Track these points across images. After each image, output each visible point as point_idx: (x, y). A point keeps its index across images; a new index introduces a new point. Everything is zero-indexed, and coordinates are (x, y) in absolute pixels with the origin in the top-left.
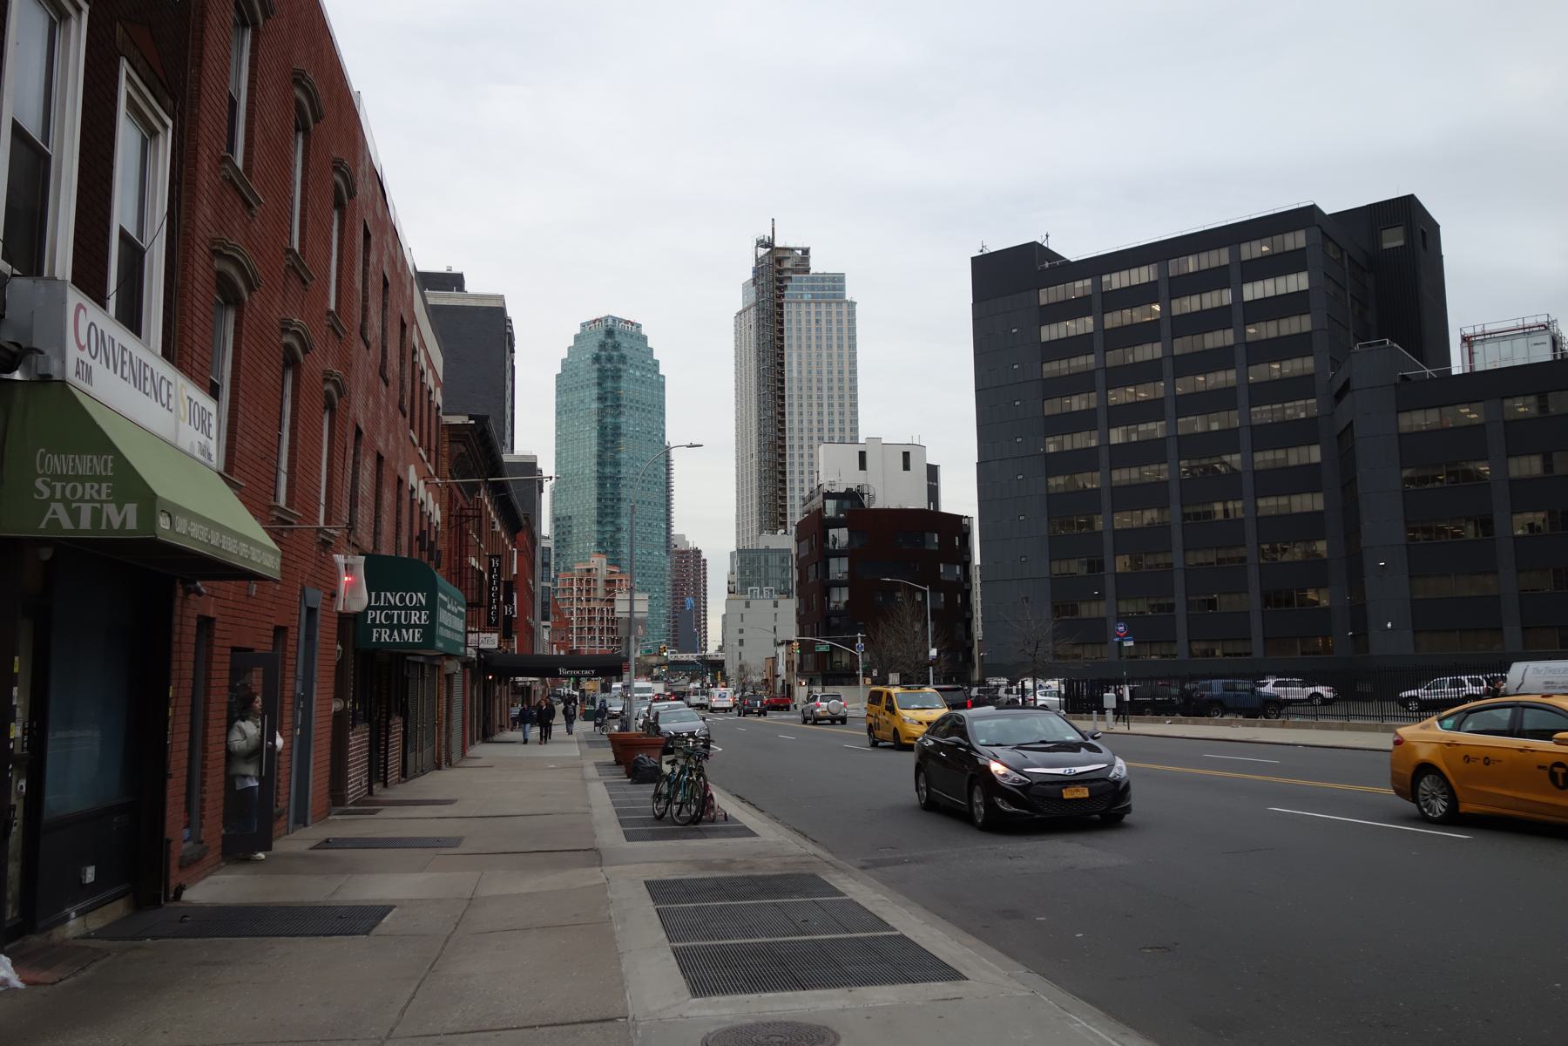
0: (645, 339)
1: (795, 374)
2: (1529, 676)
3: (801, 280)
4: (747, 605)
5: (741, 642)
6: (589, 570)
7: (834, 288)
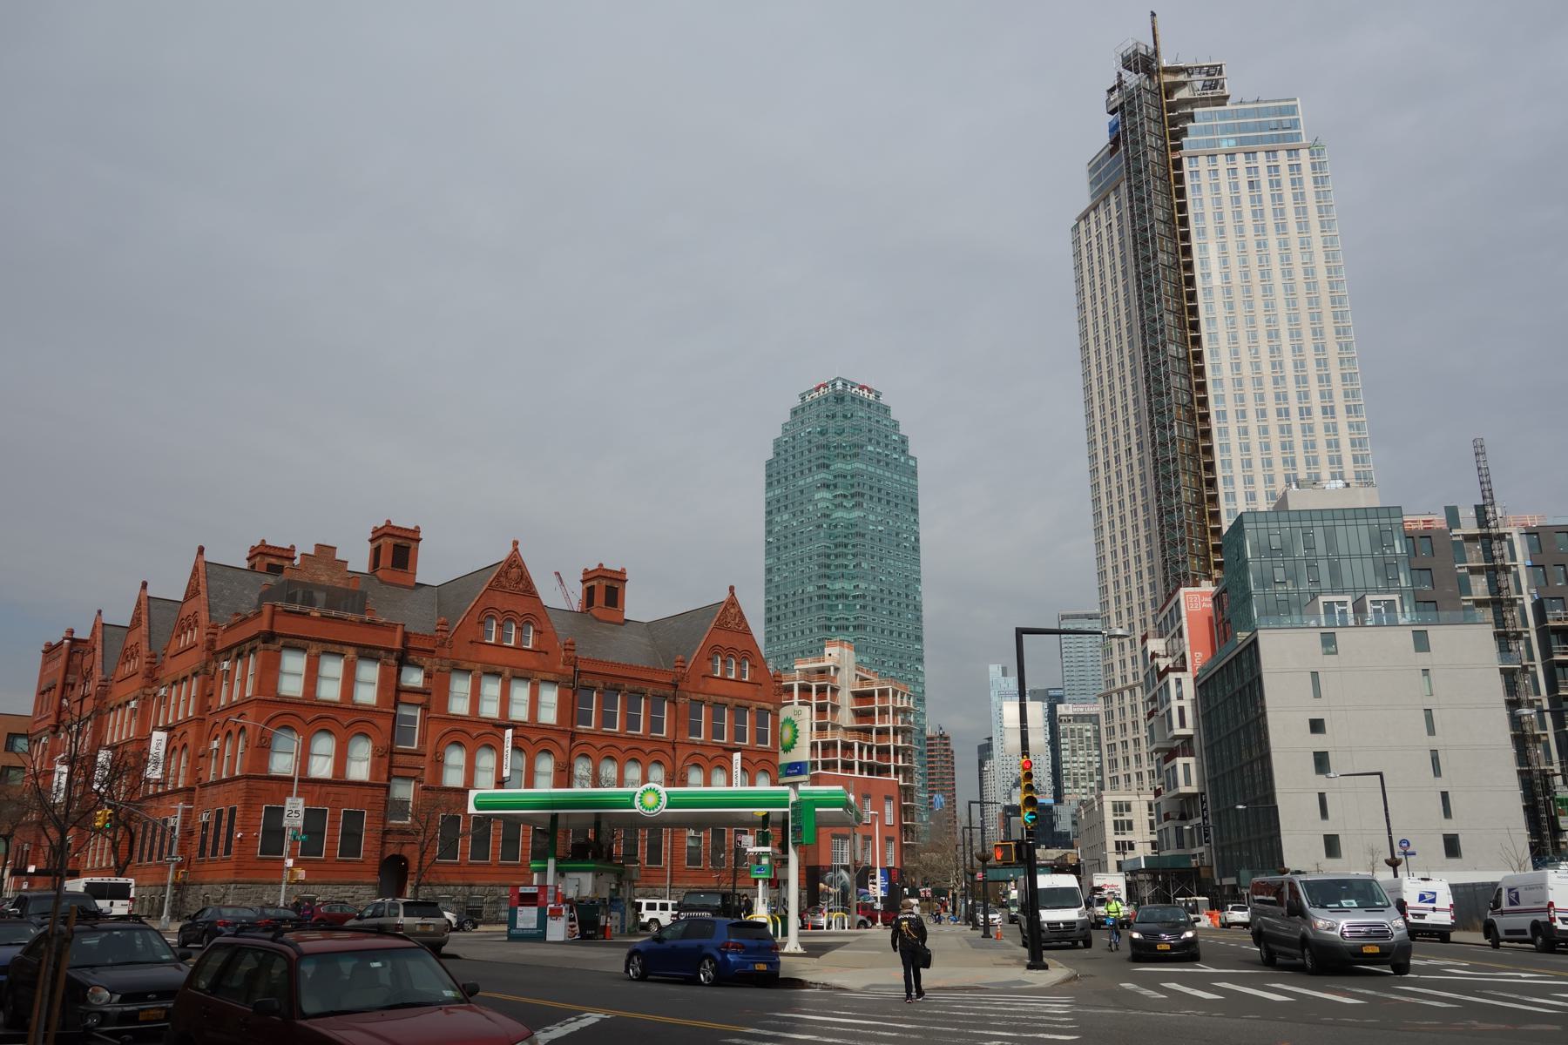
0: (887, 409)
1: (1216, 280)
2: (16, 951)
3: (1211, 117)
4: (1329, 641)
5: (1322, 762)
6: (822, 672)
7: (1280, 126)
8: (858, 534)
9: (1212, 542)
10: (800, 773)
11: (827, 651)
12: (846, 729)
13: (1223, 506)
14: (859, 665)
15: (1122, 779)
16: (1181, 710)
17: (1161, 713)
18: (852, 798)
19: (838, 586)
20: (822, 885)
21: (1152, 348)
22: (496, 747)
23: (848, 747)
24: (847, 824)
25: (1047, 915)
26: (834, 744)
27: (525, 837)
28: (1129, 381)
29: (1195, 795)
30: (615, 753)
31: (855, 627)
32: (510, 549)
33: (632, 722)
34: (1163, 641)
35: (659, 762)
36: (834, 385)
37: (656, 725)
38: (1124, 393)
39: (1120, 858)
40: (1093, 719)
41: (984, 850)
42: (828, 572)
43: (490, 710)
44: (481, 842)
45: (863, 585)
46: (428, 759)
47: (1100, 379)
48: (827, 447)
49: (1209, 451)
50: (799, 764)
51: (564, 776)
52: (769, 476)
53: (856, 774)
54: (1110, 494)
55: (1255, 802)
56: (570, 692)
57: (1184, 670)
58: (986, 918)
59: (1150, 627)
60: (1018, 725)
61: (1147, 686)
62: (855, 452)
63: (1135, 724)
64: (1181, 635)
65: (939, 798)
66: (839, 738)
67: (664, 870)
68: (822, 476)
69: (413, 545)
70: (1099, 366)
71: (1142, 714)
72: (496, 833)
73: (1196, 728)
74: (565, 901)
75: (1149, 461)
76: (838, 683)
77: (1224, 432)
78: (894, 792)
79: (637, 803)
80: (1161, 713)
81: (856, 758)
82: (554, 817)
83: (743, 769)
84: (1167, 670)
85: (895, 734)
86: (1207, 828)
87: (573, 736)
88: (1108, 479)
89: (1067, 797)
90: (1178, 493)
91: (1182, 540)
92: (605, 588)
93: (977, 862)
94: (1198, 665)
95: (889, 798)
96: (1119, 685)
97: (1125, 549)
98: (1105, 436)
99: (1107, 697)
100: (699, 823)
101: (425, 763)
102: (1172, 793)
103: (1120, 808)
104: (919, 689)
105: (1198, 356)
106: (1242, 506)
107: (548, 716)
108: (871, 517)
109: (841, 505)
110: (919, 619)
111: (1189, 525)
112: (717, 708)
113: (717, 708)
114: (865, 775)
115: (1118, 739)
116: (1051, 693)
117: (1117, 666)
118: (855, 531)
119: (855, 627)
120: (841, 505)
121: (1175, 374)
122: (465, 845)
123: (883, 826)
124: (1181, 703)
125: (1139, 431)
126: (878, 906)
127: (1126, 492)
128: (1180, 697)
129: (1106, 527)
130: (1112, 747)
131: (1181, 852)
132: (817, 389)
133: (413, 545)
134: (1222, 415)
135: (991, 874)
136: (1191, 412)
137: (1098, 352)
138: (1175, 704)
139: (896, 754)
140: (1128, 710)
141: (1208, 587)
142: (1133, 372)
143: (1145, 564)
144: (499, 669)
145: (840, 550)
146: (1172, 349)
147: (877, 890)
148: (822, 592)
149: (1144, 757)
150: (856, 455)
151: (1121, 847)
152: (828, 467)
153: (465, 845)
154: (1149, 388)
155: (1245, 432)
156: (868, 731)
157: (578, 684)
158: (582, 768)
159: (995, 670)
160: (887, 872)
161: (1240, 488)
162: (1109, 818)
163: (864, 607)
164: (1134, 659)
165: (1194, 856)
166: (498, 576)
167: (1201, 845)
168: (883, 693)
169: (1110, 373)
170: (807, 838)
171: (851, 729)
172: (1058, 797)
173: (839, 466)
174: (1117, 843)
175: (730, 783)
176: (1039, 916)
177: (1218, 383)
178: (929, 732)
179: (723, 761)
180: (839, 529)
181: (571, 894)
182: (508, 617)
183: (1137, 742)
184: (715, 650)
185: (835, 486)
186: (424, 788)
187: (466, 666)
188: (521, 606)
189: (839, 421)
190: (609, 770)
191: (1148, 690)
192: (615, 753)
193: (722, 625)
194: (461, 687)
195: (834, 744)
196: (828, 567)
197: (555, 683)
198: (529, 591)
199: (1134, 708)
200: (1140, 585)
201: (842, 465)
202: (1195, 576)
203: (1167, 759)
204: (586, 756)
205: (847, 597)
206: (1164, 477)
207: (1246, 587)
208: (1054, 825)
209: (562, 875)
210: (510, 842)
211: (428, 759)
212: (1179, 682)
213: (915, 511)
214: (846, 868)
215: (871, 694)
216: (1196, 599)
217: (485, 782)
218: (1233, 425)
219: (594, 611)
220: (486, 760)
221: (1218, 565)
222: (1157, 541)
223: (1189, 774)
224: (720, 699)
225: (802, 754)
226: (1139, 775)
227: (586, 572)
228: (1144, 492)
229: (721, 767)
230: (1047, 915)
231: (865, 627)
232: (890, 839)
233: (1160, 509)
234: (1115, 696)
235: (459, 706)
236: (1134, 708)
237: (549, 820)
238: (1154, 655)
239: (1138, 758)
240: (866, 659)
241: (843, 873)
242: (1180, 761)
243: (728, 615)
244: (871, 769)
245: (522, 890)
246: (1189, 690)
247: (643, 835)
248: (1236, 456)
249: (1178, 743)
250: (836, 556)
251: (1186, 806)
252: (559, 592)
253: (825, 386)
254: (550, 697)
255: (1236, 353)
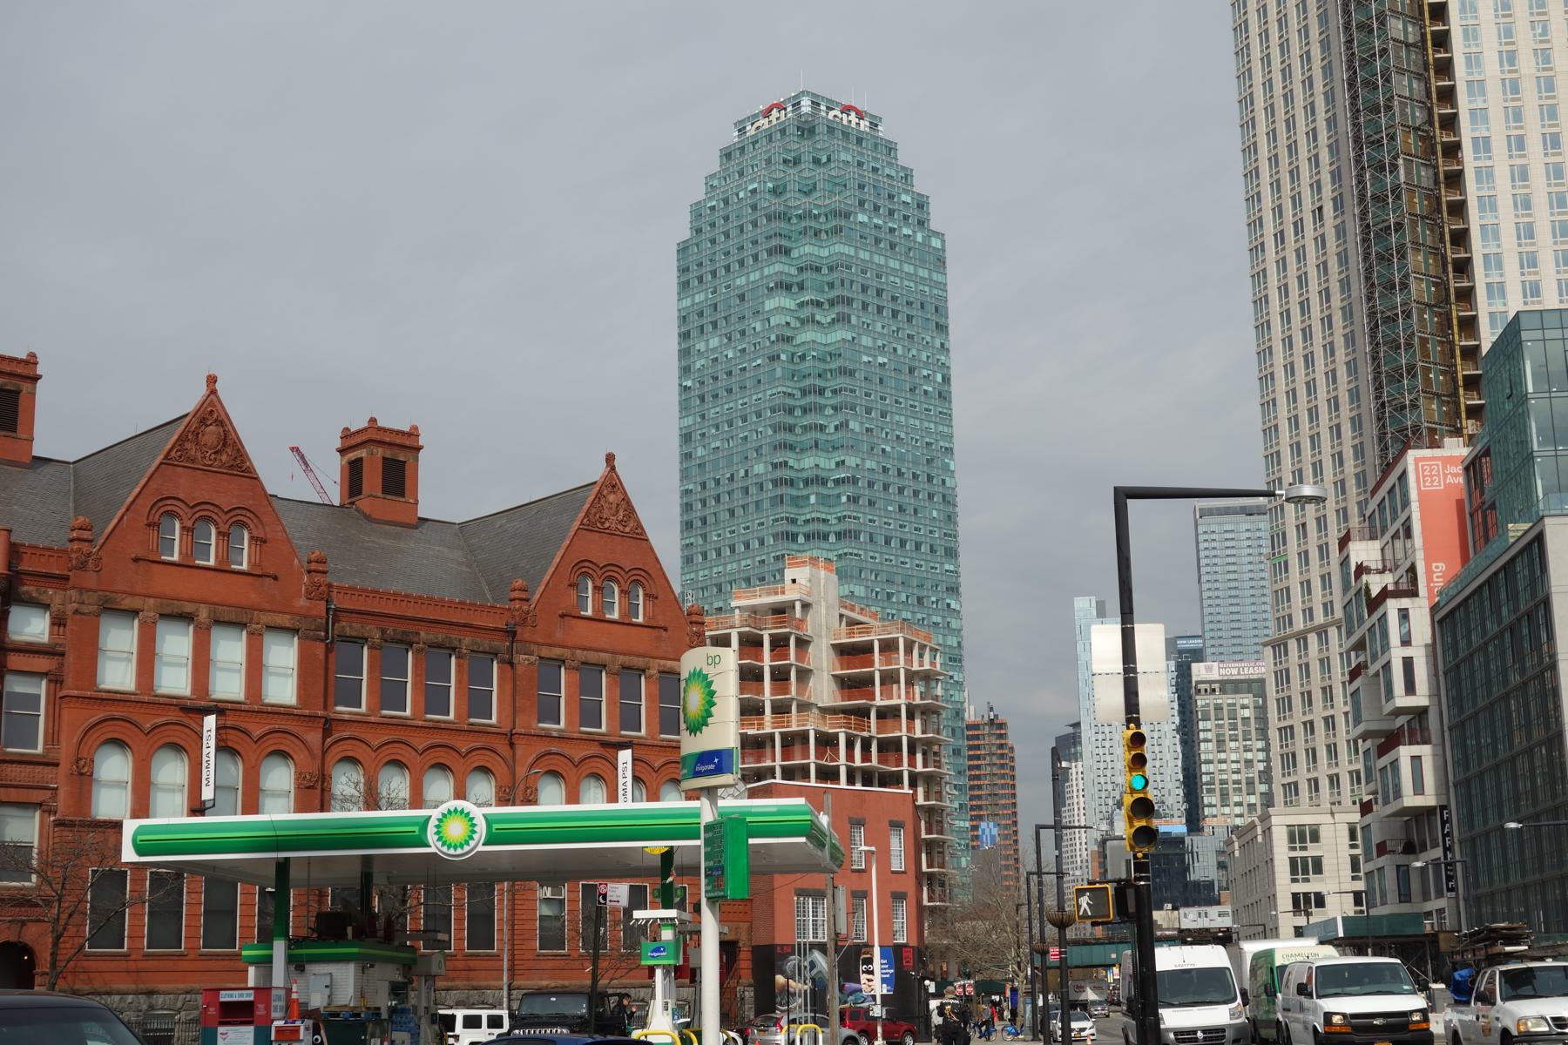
0: (891, 148)
6: (780, 611)
8: (844, 371)
9: (1463, 370)
10: (719, 770)
11: (789, 574)
12: (825, 711)
13: (1484, 307)
14: (846, 601)
15: (1304, 787)
16: (1408, 663)
17: (1372, 670)
18: (824, 820)
19: (808, 462)
20: (780, 979)
21: (1361, 26)
22: (188, 747)
23: (827, 742)
24: (821, 865)
25: (1173, 1018)
26: (804, 736)
27: (247, 904)
28: (1319, 86)
29: (1430, 811)
30: (404, 754)
31: (839, 535)
32: (202, 391)
33: (437, 700)
34: (1377, 545)
35: (485, 770)
36: (797, 105)
37: (479, 704)
38: (1311, 109)
39: (1301, 921)
40: (1255, 687)
41: (1061, 908)
42: (790, 438)
43: (175, 680)
44: (166, 914)
45: (852, 461)
46: (63, 770)
47: (1268, 84)
48: (784, 217)
49: (1459, 209)
50: (718, 753)
51: (314, 792)
52: (684, 270)
53: (843, 784)
54: (1284, 290)
55: (1537, 817)
56: (320, 649)
57: (1413, 594)
58: (1066, 1029)
59: (1355, 521)
60: (1120, 667)
61: (1348, 625)
62: (837, 223)
63: (1327, 692)
64: (1408, 533)
65: (989, 829)
66: (812, 725)
67: (498, 957)
68: (777, 268)
69: (25, 387)
70: (1266, 60)
71: (1338, 673)
72: (193, 900)
73: (1435, 693)
74: (306, 1014)
75: (1354, 229)
76: (809, 630)
77: (1486, 175)
78: (906, 815)
79: (431, 836)
80: (1372, 670)
81: (842, 759)
82: (283, 867)
83: (636, 779)
84: (1385, 594)
85: (911, 717)
86: (1450, 865)
87: (328, 726)
88: (1282, 264)
89: (1209, 822)
90: (1405, 286)
91: (1411, 369)
92: (382, 464)
93: (1051, 931)
94: (1439, 583)
95: (896, 825)
96: (1299, 624)
97: (1311, 387)
98: (1276, 185)
99: (1279, 646)
100: (554, 871)
101: (59, 778)
102: (1393, 807)
103: (1302, 836)
104: (952, 641)
105: (1442, 40)
106: (1515, 303)
107: (282, 689)
108: (866, 341)
109: (811, 320)
110: (950, 519)
111: (1424, 341)
112: (589, 670)
113: (589, 670)
114: (858, 787)
115: (1297, 718)
116: (1182, 644)
117: (1296, 591)
118: (838, 365)
119: (839, 535)
120: (811, 320)
121: (1401, 71)
122: (136, 923)
123: (886, 873)
124: (1408, 652)
125: (1336, 176)
126: (877, 1011)
127: (1314, 286)
128: (1406, 642)
129: (1278, 347)
130: (1287, 732)
131: (1405, 908)
132: (767, 113)
133: (25, 387)
134: (1483, 145)
135: (1076, 955)
136: (1428, 140)
137: (1265, 35)
138: (1397, 654)
139: (912, 752)
140: (1315, 668)
141: (1456, 449)
142: (1327, 70)
143: (1346, 411)
144: (189, 608)
145: (811, 399)
146: (1396, 27)
147: (875, 983)
148: (779, 473)
149: (1343, 749)
150: (837, 230)
151: (1302, 903)
152: (787, 252)
153: (136, 923)
154: (1354, 98)
155: (1523, 174)
156: (863, 713)
157: (336, 632)
158: (346, 781)
159: (1084, 605)
160: (895, 954)
161: (1512, 275)
162: (1282, 854)
163: (853, 500)
164: (1326, 579)
165: (1428, 915)
166: (182, 439)
167: (1439, 895)
168: (889, 647)
169: (1286, 73)
170: (736, 887)
171: (833, 711)
172: (1194, 821)
173: (806, 250)
174: (1295, 896)
175: (613, 797)
176: (1158, 1020)
177: (1477, 87)
178: (971, 715)
179: (600, 766)
180: (808, 363)
181: (317, 1001)
182: (203, 514)
183: (1330, 722)
184: (582, 569)
185: (801, 287)
186: (59, 824)
187: (128, 603)
188: (227, 494)
189: (807, 170)
190: (396, 784)
191: (1349, 633)
192: (404, 754)
193: (593, 525)
194: (118, 645)
195: (804, 736)
196: (791, 429)
197: (294, 631)
198: (238, 465)
199: (1325, 663)
200: (1328, 474)
201: (811, 248)
202: (1432, 431)
203: (1383, 750)
204: (353, 761)
205: (824, 482)
206: (1381, 258)
207: (1524, 443)
208: (1186, 869)
209: (301, 968)
210: (220, 917)
211: (63, 770)
212: (1404, 615)
213: (942, 328)
214: (822, 948)
215: (866, 649)
216: (1436, 470)
217: (154, 809)
218: (1501, 163)
219: (363, 503)
220: (171, 771)
221: (1474, 412)
222: (1366, 370)
223: (1420, 776)
224: (593, 657)
225: (724, 732)
226: (1334, 780)
227: (347, 434)
228: (1345, 285)
229: (597, 777)
230: (1173, 1018)
231: (857, 536)
232: (899, 896)
233: (1372, 314)
234: (1292, 645)
235: (117, 675)
236: (1325, 663)
237: (272, 872)
238: (1361, 570)
239: (1332, 750)
240: (860, 591)
241: (817, 956)
242: (1405, 752)
243: (605, 509)
244: (868, 777)
245: (225, 997)
246: (1422, 628)
247: (459, 897)
248: (1507, 217)
249: (1401, 721)
250: (805, 411)
251: (1415, 829)
252: (295, 462)
253: (781, 107)
254: (283, 656)
255: (1509, 33)
